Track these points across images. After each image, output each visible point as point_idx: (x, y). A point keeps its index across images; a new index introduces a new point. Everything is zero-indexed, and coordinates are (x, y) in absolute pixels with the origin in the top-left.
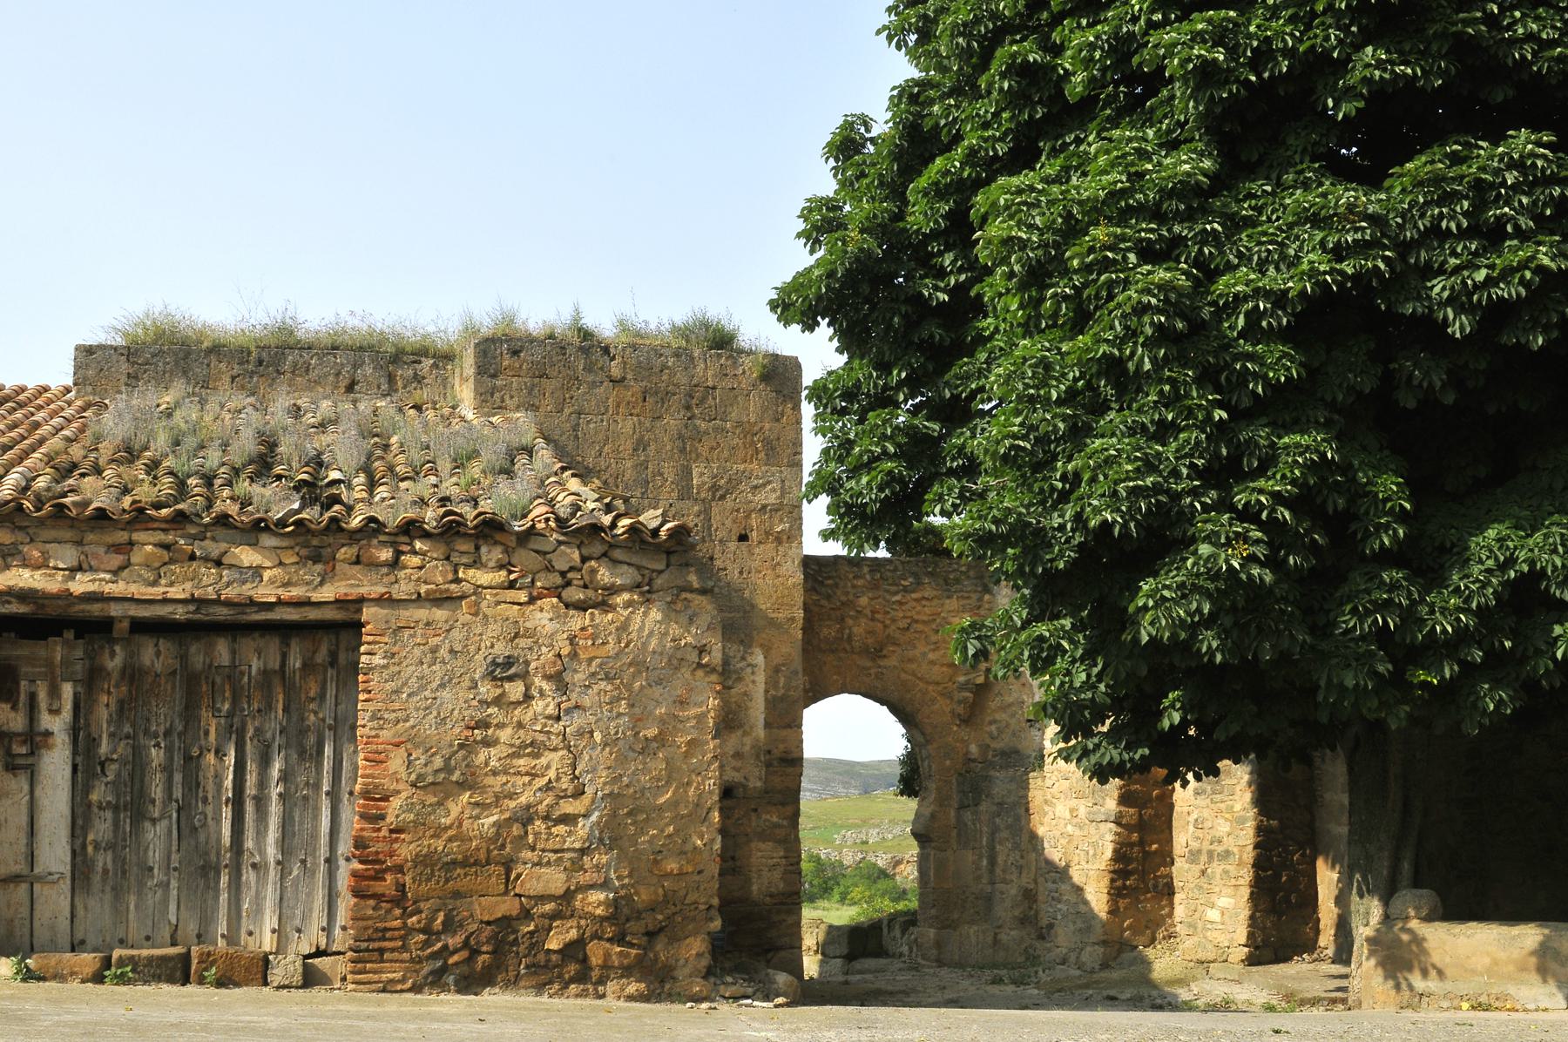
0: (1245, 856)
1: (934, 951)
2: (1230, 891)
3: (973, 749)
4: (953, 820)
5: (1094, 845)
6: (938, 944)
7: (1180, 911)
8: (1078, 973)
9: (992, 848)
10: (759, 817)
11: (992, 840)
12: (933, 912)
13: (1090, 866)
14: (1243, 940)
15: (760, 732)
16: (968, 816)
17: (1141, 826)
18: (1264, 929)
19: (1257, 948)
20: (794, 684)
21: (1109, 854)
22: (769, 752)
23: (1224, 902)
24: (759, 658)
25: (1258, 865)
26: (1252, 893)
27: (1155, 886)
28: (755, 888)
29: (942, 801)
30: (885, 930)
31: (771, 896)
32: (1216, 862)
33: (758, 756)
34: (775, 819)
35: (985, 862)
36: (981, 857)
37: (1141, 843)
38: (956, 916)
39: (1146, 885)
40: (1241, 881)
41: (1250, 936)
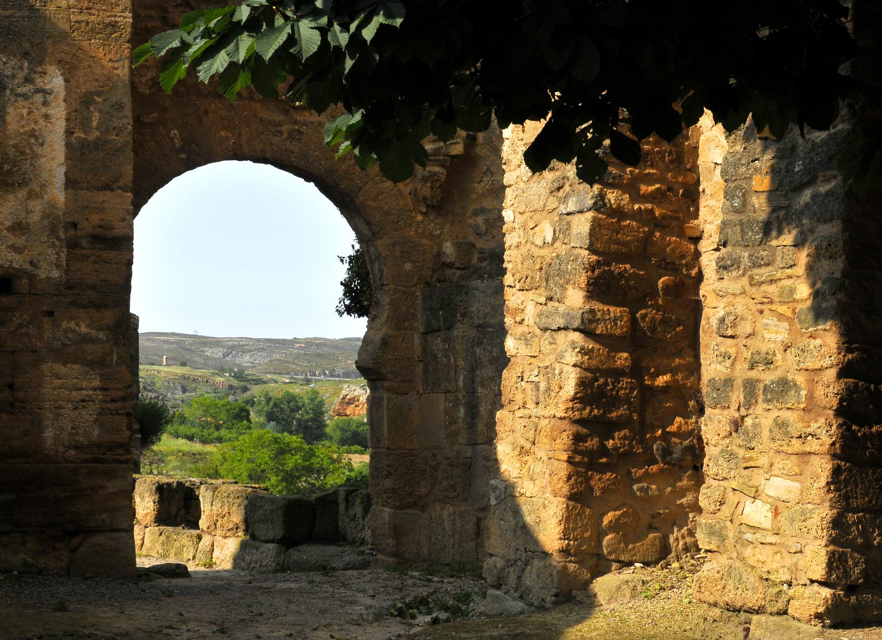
0: (820, 391)
1: (391, 541)
2: (790, 464)
3: (448, 248)
4: (418, 351)
5: (546, 371)
6: (397, 531)
7: (706, 497)
8: (519, 605)
9: (472, 392)
10: (56, 325)
11: (471, 380)
12: (388, 483)
13: (540, 411)
14: (819, 572)
15: (58, 194)
16: (437, 344)
17: (634, 339)
18: (866, 548)
19: (851, 589)
20: (117, 123)
21: (570, 388)
22: (74, 225)
23: (779, 486)
24: (56, 81)
25: (848, 411)
26: (836, 472)
27: (666, 452)
28: (49, 435)
29: (400, 321)
30: (342, 506)
31: (78, 447)
32: (761, 406)
33: (53, 231)
34: (84, 329)
35: (462, 412)
36: (456, 407)
37: (636, 371)
38: (423, 491)
39: (648, 449)
40: (813, 445)
41: (834, 562)
